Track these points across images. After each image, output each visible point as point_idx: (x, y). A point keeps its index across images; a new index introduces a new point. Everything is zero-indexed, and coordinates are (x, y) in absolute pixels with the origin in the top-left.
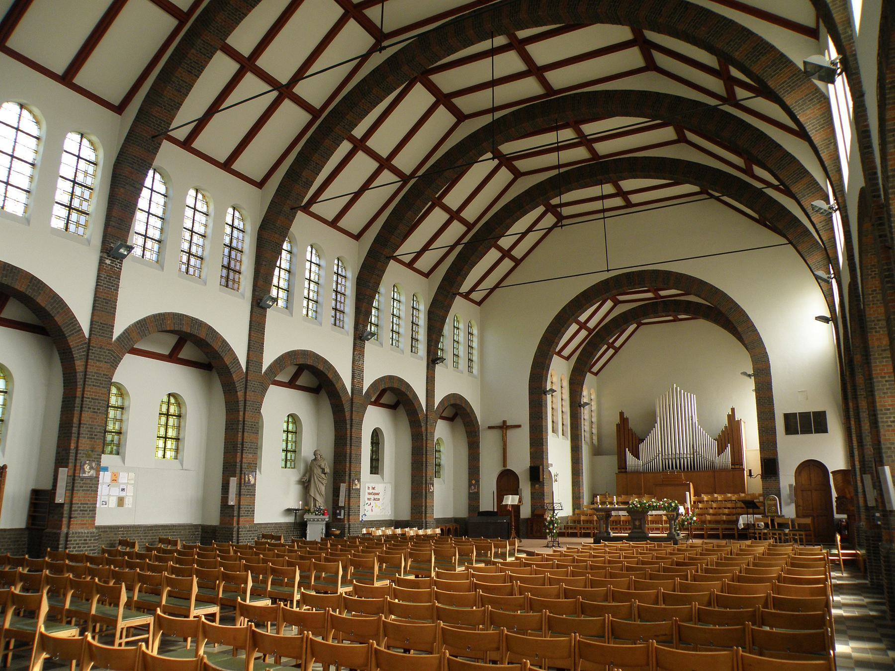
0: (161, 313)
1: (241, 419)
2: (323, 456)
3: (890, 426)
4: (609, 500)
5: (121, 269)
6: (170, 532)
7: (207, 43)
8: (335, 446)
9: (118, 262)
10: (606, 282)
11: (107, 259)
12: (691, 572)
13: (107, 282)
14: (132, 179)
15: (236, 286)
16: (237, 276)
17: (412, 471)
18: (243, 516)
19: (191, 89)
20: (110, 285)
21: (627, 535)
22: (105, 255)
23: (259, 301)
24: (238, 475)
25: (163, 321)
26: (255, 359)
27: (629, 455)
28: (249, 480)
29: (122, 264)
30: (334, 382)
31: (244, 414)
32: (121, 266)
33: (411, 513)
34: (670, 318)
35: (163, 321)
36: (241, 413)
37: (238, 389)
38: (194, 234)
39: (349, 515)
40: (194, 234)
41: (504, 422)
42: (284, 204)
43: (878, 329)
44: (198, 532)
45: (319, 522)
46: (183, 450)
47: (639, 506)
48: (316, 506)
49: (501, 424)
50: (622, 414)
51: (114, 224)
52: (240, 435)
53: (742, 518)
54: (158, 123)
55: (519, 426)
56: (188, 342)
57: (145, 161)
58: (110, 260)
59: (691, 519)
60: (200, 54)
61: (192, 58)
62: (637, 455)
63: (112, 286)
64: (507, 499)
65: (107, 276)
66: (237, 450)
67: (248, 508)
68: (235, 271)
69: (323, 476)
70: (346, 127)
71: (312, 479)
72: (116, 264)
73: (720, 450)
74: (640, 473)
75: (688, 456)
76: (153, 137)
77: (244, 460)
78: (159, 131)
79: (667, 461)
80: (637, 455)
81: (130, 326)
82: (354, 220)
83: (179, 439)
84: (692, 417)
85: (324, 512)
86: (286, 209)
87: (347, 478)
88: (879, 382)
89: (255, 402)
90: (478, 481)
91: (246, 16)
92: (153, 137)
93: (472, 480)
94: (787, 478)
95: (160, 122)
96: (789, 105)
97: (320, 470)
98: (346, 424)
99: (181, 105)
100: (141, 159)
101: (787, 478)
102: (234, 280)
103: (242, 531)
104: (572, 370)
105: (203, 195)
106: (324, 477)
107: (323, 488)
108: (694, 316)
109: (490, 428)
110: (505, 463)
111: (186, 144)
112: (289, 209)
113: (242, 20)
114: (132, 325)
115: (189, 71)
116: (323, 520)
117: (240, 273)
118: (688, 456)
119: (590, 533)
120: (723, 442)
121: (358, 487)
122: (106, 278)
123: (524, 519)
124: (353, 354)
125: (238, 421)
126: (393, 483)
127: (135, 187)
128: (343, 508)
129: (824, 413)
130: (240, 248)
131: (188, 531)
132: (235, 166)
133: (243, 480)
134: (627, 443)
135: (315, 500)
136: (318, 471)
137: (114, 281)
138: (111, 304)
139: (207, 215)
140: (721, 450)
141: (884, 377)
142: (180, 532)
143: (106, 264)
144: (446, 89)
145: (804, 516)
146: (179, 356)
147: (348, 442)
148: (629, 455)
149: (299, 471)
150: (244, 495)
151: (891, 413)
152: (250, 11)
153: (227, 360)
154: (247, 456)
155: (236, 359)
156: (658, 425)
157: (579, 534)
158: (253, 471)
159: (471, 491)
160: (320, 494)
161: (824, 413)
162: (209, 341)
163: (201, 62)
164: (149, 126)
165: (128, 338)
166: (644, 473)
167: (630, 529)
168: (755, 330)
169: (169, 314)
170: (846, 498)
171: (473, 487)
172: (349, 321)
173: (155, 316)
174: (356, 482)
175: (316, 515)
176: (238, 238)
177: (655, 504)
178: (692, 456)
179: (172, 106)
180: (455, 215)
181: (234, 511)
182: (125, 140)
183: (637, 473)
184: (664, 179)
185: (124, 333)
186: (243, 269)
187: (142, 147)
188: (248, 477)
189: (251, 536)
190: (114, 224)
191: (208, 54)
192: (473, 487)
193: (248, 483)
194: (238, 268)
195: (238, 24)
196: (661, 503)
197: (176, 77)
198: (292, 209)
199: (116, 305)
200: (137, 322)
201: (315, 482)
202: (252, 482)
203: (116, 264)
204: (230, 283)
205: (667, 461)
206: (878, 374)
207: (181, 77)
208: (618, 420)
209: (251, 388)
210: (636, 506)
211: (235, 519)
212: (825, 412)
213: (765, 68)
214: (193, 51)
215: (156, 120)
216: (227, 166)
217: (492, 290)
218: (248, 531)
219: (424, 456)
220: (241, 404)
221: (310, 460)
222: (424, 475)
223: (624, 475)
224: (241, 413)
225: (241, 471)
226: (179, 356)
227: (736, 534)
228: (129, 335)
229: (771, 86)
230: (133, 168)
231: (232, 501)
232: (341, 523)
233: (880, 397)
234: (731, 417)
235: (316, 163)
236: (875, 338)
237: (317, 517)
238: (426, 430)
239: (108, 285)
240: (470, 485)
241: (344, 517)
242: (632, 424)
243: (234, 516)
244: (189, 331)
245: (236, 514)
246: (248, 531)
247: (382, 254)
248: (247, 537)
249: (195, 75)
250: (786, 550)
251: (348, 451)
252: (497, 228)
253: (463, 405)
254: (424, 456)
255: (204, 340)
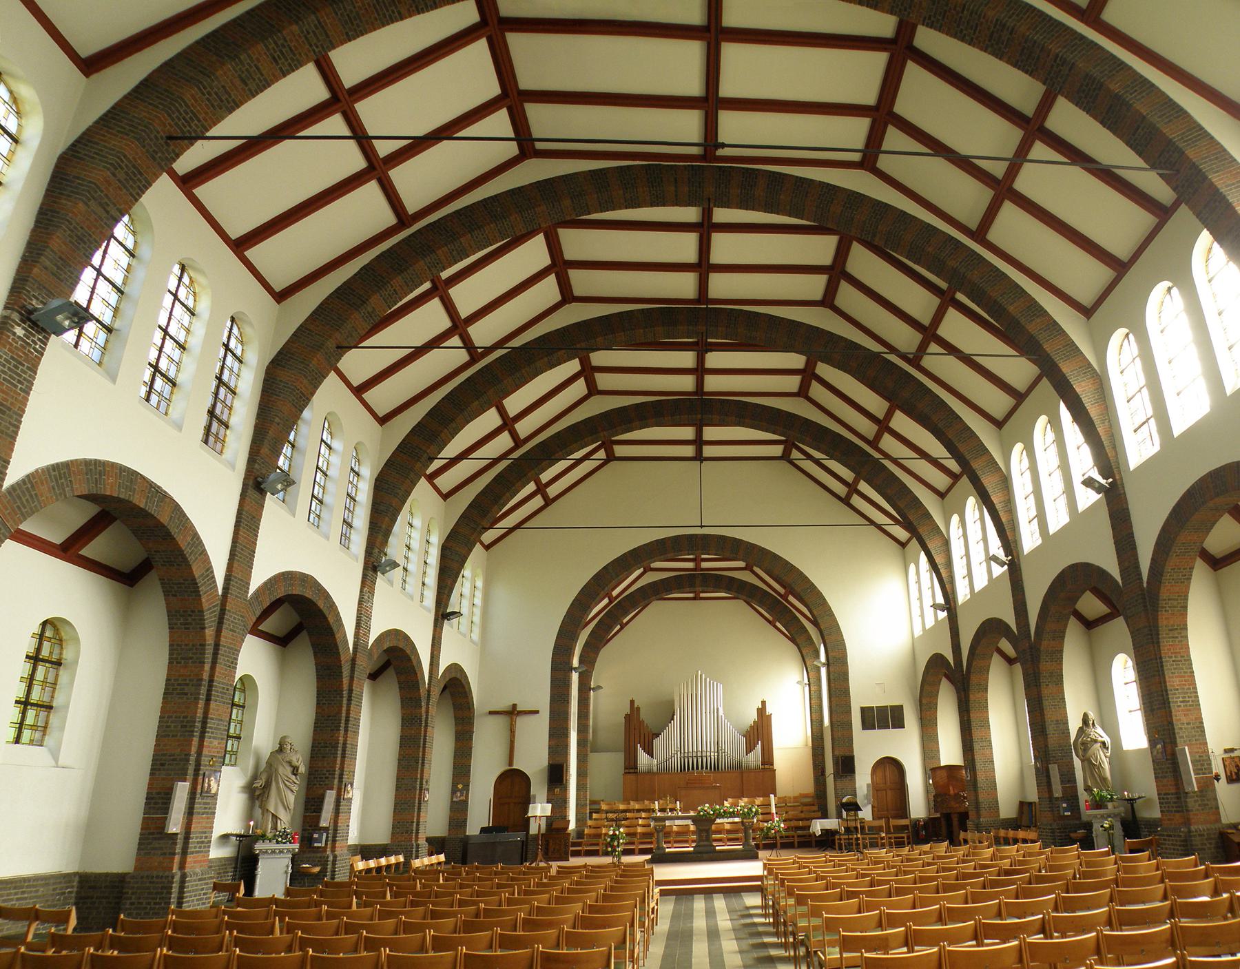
0: (100, 461)
1: (206, 676)
2: (295, 747)
3: (1180, 706)
4: (670, 806)
5: (42, 355)
6: (16, 894)
7: (323, 27)
8: (314, 731)
9: (39, 339)
10: (676, 539)
11: (19, 325)
12: (505, 896)
13: (9, 369)
14: (106, 195)
15: (219, 445)
16: (222, 429)
17: (399, 770)
18: (192, 853)
19: (265, 88)
20: (14, 379)
21: (692, 849)
22: (16, 316)
23: (260, 479)
24: (190, 777)
25: (100, 475)
26: (239, 576)
27: (641, 752)
28: (209, 785)
29: (46, 345)
30: (335, 628)
31: (213, 668)
32: (44, 349)
33: (392, 833)
34: (691, 595)
35: (100, 475)
36: (207, 667)
37: (207, 623)
38: (167, 337)
39: (334, 841)
40: (167, 337)
41: (514, 706)
42: (330, 337)
43: (1167, 609)
44: (72, 887)
45: (273, 856)
46: (62, 729)
47: (712, 812)
48: (276, 829)
49: (510, 709)
50: (632, 702)
51: (48, 263)
52: (201, 704)
53: (820, 823)
54: (187, 117)
55: (537, 712)
56: (117, 524)
57: (141, 174)
58: (23, 328)
59: (779, 826)
60: (303, 39)
61: (288, 39)
62: (650, 752)
63: (19, 382)
64: (535, 808)
65: (12, 358)
66: (193, 731)
67: (201, 837)
68: (221, 422)
69: (293, 777)
70: (455, 253)
71: (274, 784)
72: (33, 341)
73: (748, 750)
74: (654, 774)
75: (712, 754)
76: (170, 138)
77: (205, 751)
78: (195, 131)
79: (686, 760)
80: (650, 752)
81: (37, 471)
82: (385, 396)
83: (51, 708)
84: (718, 709)
85: (293, 838)
86: (331, 344)
87: (336, 781)
88: (1167, 661)
89: (232, 648)
90: (466, 787)
91: (402, 19)
92: (170, 138)
93: (458, 784)
94: (863, 779)
95: (191, 118)
96: (1065, 372)
97: (289, 769)
98: (342, 697)
99: (238, 107)
100: (134, 166)
101: (863, 779)
102: (217, 436)
103: (190, 881)
104: (584, 646)
105: (191, 278)
106: (296, 781)
107: (291, 798)
108: (736, 595)
109: (491, 713)
110: (511, 760)
111: (188, 182)
112: (335, 346)
113: (393, 22)
114: (43, 469)
115: (274, 58)
116: (288, 851)
117: (227, 427)
118: (712, 754)
119: (634, 849)
120: (752, 742)
121: (350, 796)
122: (10, 363)
123: (1005, 819)
124: (361, 591)
125: (201, 680)
126: (362, 790)
127: (107, 212)
128: (326, 829)
129: (900, 708)
130: (232, 385)
131: (51, 888)
132: (251, 254)
133: (199, 787)
134: (637, 739)
135: (275, 817)
136: (285, 771)
137: (25, 373)
138: (11, 417)
139: (193, 314)
140: (750, 748)
141: (1171, 657)
142: (37, 891)
143: (14, 334)
144: (570, 254)
145: (880, 818)
146: (83, 552)
147: (343, 725)
148: (641, 752)
149: (244, 770)
150: (199, 813)
151: (1179, 693)
152: (411, 16)
153: (197, 571)
154: (211, 742)
155: (209, 570)
156: (677, 717)
157: (637, 851)
158: (216, 771)
159: (454, 799)
160: (286, 808)
161: (900, 708)
162: (174, 531)
163: (300, 54)
164: (169, 115)
165: (29, 492)
166: (657, 773)
167: (693, 841)
168: (831, 615)
169: (113, 465)
170: (949, 795)
171: (459, 794)
172: (359, 541)
173: (88, 463)
174: (349, 788)
175: (278, 842)
176: (231, 370)
177: (731, 810)
178: (716, 754)
179: (222, 101)
180: (508, 424)
181: (176, 844)
182: (97, 122)
183: (649, 773)
184: (774, 433)
185: (23, 481)
186: (233, 421)
187: (144, 147)
188: (209, 781)
189: (202, 889)
190: (48, 263)
191: (317, 47)
192: (459, 794)
193: (207, 792)
194: (225, 418)
195: (384, 26)
196: (739, 808)
197: (249, 56)
198: (338, 347)
199: (20, 422)
200: (53, 465)
201: (278, 788)
202: (213, 791)
203: (33, 341)
204: (211, 439)
205: (686, 760)
206: (1166, 653)
207: (258, 60)
208: (628, 711)
209: (229, 625)
210: (708, 813)
211: (177, 859)
212: (902, 706)
213: (1040, 330)
214: (295, 28)
215: (185, 111)
216: (240, 245)
217: (511, 530)
218: (200, 880)
219: (421, 749)
220: (209, 651)
221: (266, 754)
222: (419, 777)
223: (632, 777)
224: (207, 667)
225: (197, 770)
226: (83, 552)
227: (796, 843)
228: (32, 486)
229: (1047, 349)
230: (114, 175)
231: (175, 825)
232: (319, 855)
233: (1169, 677)
234: (762, 711)
235: (395, 290)
236: (195, 682)
237: (281, 846)
238: (427, 712)
239: (10, 376)
240: (454, 791)
241: (326, 844)
242: (643, 716)
243: (174, 854)
244: (142, 506)
245: (178, 849)
246: (200, 880)
247: (425, 452)
248: (197, 890)
249: (281, 69)
250: (1010, 851)
251: (341, 739)
252: (558, 452)
253: (463, 680)
254: (421, 749)
255: (164, 526)
